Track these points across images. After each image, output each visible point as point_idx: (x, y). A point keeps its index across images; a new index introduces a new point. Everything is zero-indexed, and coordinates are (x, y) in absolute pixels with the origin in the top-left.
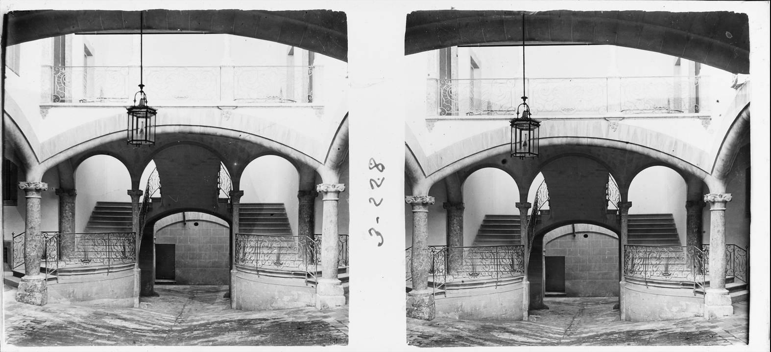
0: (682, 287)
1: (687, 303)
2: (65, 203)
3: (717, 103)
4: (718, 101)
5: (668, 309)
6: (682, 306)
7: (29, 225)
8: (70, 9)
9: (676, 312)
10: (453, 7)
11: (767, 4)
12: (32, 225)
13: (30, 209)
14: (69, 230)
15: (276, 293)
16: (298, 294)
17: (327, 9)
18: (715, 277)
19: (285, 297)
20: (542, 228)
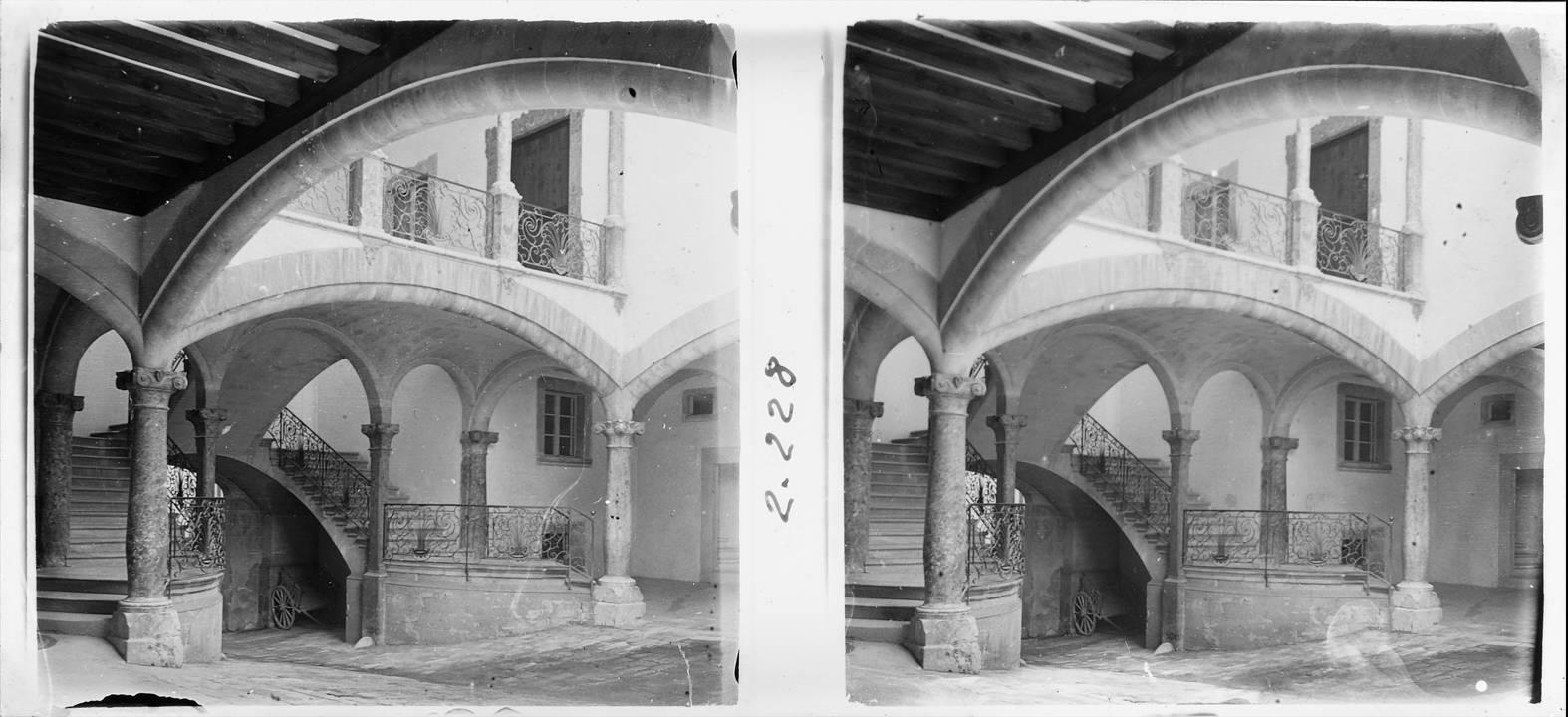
0: (532, 575)
1: (1354, 608)
2: (857, 436)
3: (1458, 210)
4: (1460, 206)
5: (1319, 620)
6: (545, 608)
7: (951, 480)
8: (656, 19)
9: (535, 620)
10: (921, 14)
11: (1563, 5)
12: (958, 480)
13: (953, 442)
14: (65, 492)
15: (1312, 612)
16: (553, 604)
17: (696, 20)
18: (621, 556)
19: (530, 613)
20: (208, 464)
